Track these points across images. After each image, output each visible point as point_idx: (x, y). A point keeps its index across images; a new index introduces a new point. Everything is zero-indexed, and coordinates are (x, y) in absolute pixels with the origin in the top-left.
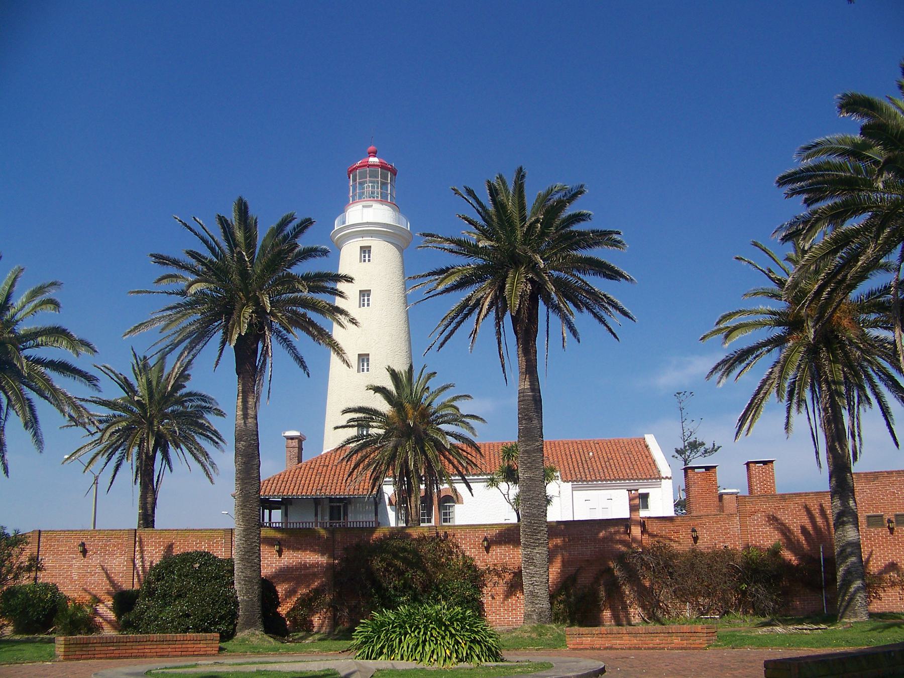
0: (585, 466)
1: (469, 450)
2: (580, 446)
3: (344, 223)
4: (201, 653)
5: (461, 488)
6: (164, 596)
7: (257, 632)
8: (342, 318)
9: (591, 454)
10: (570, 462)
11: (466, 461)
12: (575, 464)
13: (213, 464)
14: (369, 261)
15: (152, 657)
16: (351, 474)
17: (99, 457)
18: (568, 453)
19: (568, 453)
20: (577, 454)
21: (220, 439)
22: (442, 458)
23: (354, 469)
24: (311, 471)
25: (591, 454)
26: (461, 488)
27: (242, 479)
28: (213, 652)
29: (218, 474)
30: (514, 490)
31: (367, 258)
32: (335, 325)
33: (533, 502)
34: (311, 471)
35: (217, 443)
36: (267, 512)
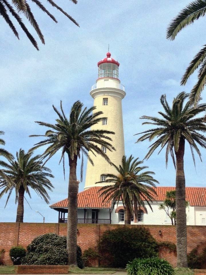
0: (200, 200)
1: (152, 193)
2: (198, 190)
3: (96, 87)
4: (63, 272)
5: (147, 206)
6: (40, 251)
7: (75, 266)
8: (110, 147)
9: (203, 194)
10: (194, 197)
11: (151, 196)
12: (196, 198)
13: (48, 196)
14: (107, 105)
15: (46, 273)
16: (103, 201)
17: (5, 193)
18: (193, 193)
19: (193, 193)
20: (197, 194)
21: (52, 186)
22: (141, 195)
23: (104, 199)
24: (83, 197)
25: (203, 194)
26: (147, 206)
27: (71, 206)
28: (67, 272)
29: (50, 199)
30: (171, 210)
31: (106, 103)
32: (107, 150)
33: (180, 217)
34: (83, 197)
35: (49, 188)
36: (63, 213)
